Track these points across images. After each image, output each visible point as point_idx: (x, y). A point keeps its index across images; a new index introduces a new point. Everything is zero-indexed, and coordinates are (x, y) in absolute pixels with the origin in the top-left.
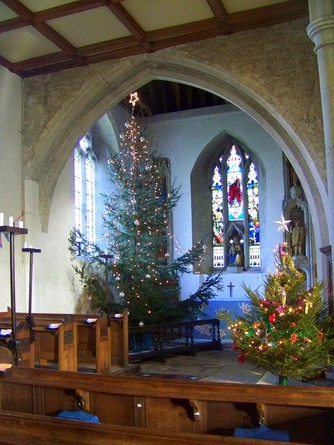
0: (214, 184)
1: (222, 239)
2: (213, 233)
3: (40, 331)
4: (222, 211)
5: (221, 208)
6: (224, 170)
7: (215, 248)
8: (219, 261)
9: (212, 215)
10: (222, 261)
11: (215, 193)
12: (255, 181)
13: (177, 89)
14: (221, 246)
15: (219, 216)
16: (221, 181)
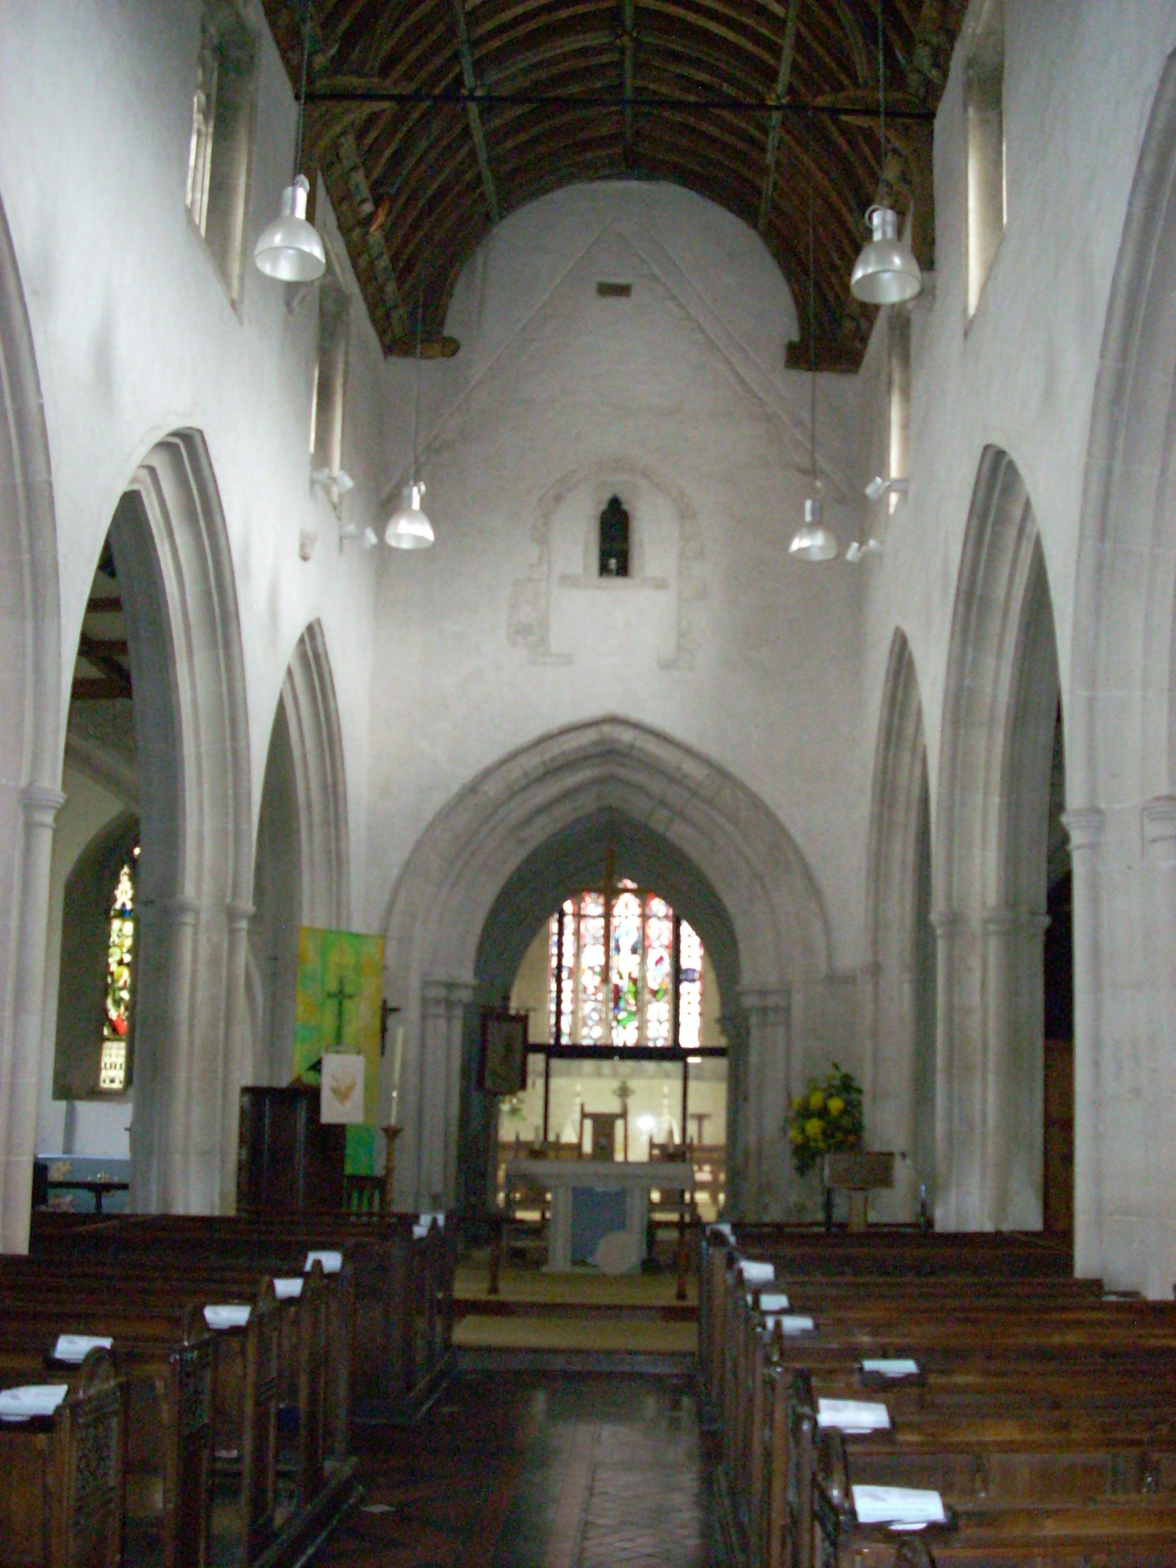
0: (118, 906)
1: (124, 1026)
3: (125, 1432)
4: (128, 965)
5: (127, 958)
6: (789, 1311)
7: (107, 1044)
10: (120, 1075)
11: (116, 924)
12: (129, 906)
13: (78, 703)
14: (119, 1040)
16: (132, 900)
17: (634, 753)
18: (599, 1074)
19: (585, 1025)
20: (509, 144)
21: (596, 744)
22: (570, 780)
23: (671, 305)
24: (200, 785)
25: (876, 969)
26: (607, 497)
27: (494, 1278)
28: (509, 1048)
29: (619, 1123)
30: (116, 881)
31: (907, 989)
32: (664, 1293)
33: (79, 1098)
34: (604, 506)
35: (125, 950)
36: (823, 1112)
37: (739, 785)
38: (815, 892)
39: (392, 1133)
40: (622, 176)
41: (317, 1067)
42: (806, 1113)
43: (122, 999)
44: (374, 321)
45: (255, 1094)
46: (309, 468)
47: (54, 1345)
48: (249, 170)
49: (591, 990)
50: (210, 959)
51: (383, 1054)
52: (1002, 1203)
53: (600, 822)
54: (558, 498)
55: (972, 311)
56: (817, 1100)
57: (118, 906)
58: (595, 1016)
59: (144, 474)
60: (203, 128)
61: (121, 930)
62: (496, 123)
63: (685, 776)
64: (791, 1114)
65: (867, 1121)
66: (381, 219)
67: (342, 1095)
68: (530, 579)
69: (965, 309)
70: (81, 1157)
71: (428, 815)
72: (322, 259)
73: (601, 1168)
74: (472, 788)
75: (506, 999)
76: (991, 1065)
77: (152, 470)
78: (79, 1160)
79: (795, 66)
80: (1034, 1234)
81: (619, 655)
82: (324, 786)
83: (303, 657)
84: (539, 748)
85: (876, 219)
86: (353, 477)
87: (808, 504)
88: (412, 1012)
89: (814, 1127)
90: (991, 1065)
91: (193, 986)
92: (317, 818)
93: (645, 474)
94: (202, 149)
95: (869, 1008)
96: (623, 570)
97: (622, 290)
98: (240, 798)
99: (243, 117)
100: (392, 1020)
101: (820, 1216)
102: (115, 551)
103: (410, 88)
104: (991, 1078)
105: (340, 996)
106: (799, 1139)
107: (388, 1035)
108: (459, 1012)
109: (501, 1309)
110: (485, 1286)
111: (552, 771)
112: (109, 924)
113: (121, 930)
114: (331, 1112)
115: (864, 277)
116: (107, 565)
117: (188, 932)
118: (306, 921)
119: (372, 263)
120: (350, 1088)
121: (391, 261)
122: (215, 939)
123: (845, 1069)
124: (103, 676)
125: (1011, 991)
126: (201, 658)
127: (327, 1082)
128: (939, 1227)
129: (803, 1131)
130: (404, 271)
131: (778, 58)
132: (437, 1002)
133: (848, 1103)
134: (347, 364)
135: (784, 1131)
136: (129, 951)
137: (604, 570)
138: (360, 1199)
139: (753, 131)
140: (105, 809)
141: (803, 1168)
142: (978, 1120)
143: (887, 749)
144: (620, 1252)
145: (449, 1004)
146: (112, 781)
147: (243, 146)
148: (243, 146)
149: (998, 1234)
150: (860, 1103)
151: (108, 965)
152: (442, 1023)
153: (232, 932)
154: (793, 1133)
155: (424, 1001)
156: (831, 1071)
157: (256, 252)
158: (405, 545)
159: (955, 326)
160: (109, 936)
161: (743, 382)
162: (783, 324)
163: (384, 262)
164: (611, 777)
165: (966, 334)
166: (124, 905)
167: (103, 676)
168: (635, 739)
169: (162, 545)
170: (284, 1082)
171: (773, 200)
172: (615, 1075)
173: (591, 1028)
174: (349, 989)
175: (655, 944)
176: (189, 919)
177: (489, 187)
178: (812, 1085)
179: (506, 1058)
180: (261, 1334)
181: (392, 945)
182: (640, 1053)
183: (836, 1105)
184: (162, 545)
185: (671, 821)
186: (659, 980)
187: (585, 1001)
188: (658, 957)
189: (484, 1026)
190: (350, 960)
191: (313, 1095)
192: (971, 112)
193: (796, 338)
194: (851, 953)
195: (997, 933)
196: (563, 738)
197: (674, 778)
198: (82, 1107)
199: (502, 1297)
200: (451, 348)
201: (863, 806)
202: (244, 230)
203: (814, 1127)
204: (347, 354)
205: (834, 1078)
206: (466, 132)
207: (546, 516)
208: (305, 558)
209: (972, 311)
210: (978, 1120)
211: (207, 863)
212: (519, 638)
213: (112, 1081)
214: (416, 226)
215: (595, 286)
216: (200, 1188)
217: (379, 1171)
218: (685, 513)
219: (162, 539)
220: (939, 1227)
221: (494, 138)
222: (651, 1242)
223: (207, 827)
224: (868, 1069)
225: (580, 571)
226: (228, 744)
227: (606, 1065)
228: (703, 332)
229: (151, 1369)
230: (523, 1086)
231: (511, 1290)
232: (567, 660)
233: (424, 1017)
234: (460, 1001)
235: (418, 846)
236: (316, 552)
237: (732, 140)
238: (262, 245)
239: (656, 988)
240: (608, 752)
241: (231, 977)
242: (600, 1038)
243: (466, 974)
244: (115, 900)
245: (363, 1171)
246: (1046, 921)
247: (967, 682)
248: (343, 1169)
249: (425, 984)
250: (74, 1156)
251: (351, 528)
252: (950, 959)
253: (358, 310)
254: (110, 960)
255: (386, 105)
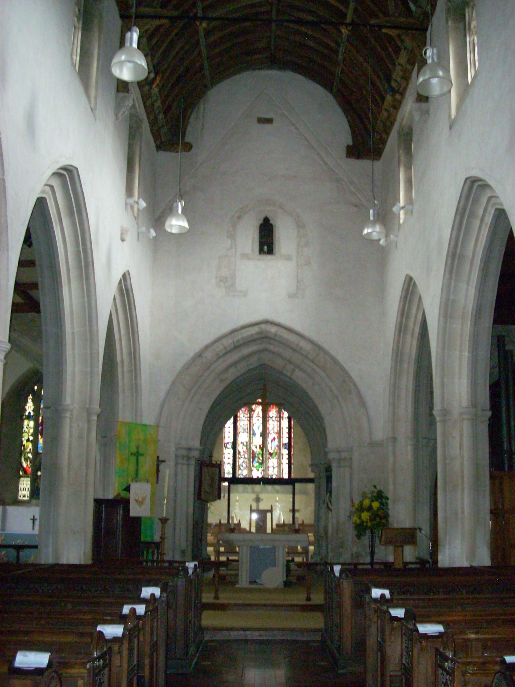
0: (27, 413)
1: (29, 470)
2: (21, 464)
4: (32, 441)
5: (31, 438)
7: (22, 479)
8: (24, 493)
9: (22, 445)
10: (27, 493)
11: (26, 422)
12: (32, 414)
14: (28, 477)
15: (30, 446)
17: (277, 338)
18: (244, 491)
19: (240, 469)
20: (217, 50)
21: (258, 333)
22: (246, 351)
23: (292, 128)
24: (73, 349)
25: (394, 439)
26: (262, 217)
27: (217, 592)
28: (212, 479)
29: (269, 515)
30: (26, 402)
31: (410, 449)
32: (298, 597)
33: (9, 505)
34: (261, 222)
35: (30, 434)
36: (370, 508)
37: (326, 352)
38: (363, 403)
39: (164, 521)
40: (269, 68)
41: (128, 489)
42: (361, 509)
43: (29, 457)
44: (152, 133)
45: (98, 502)
46: (125, 197)
47: (14, 657)
48: (99, 48)
49: (242, 453)
50: (76, 435)
51: (157, 482)
52: (473, 553)
53: (259, 372)
54: (239, 218)
55: (453, 117)
56: (366, 503)
57: (27, 413)
58: (244, 465)
59: (48, 189)
60: (77, 25)
61: (28, 425)
62: (211, 39)
63: (301, 348)
64: (354, 509)
65: (390, 513)
66: (158, 81)
67: (140, 503)
68: (226, 256)
69: (450, 116)
70: (9, 532)
71: (179, 368)
72: (146, 67)
73: (260, 536)
74: (199, 355)
75: (211, 456)
76: (466, 485)
77: (52, 187)
78: (9, 534)
79: (355, 10)
80: (488, 567)
81: (270, 292)
82: (130, 354)
83: (120, 289)
84: (233, 335)
85: (429, 53)
86: (146, 202)
87: (371, 212)
88: (171, 462)
89: (365, 516)
90: (466, 485)
91: (70, 448)
92: (126, 368)
93: (281, 207)
94: (76, 34)
95: (391, 460)
96: (270, 252)
97: (269, 121)
98: (93, 354)
99: (96, 21)
100: (162, 466)
101: (368, 560)
102: (32, 231)
103: (175, 13)
104: (466, 491)
105: (137, 455)
106: (358, 521)
107: (160, 474)
108: (193, 462)
109: (222, 607)
110: (213, 595)
111: (236, 347)
112: (23, 422)
113: (28, 425)
114: (134, 511)
115: (423, 81)
116: (28, 240)
117: (68, 421)
118: (121, 419)
119: (153, 105)
120: (144, 499)
121: (162, 103)
122: (81, 426)
123: (378, 488)
124: (23, 301)
125: (475, 449)
126: (74, 285)
127: (132, 496)
128: (440, 565)
129: (360, 517)
130: (167, 111)
131: (347, 7)
132: (183, 457)
133: (382, 504)
134: (140, 151)
135: (350, 517)
136: (32, 435)
137: (261, 251)
138: (148, 553)
139: (333, 45)
140: (24, 366)
141: (359, 536)
142: (460, 511)
143: (399, 336)
144: (273, 577)
145: (189, 458)
146: (26, 353)
147: (96, 35)
148: (96, 35)
149: (472, 567)
150: (387, 504)
151: (22, 442)
152: (185, 467)
153: (89, 421)
154: (355, 518)
155: (176, 456)
156: (373, 489)
157: (112, 63)
158: (174, 231)
159: (444, 125)
160: (23, 428)
161: (326, 164)
162: (345, 137)
163: (158, 104)
164: (265, 350)
165: (451, 128)
166: (30, 413)
167: (23, 301)
168: (277, 331)
169: (56, 226)
170: (111, 496)
171: (341, 79)
172: (253, 492)
173: (242, 471)
174: (141, 451)
175: (272, 432)
176: (68, 414)
177: (207, 72)
178: (364, 496)
179: (211, 486)
180: (130, 641)
181: (161, 430)
182: (266, 481)
183: (376, 505)
184: (56, 226)
185: (294, 370)
186: (273, 448)
187: (240, 458)
188: (272, 438)
189: (201, 470)
190: (142, 437)
191: (126, 503)
192: (450, 23)
193: (351, 143)
194: (380, 433)
195: (468, 419)
196: (243, 331)
197: (295, 350)
198: (10, 509)
199: (221, 601)
200: (188, 147)
201: (388, 362)
202: (97, 75)
203: (365, 516)
204: (141, 147)
205: (375, 492)
206: (198, 42)
207: (234, 226)
208: (123, 240)
209: (453, 117)
210: (460, 511)
211: (77, 387)
212: (222, 284)
213: (24, 496)
214: (174, 85)
215: (256, 119)
216: (74, 549)
217: (157, 538)
218: (300, 225)
219: (56, 224)
220: (440, 565)
221: (210, 47)
222: (288, 570)
223: (77, 369)
224: (391, 487)
225: (250, 251)
226: (88, 328)
227: (249, 487)
228: (307, 140)
229: (75, 671)
230: (219, 498)
231: (225, 598)
232: (245, 294)
233: (176, 464)
234: (194, 457)
235: (173, 383)
236: (128, 237)
237: (320, 48)
238: (115, 60)
239: (271, 451)
240: (264, 337)
241: (88, 444)
242: (247, 475)
243: (196, 444)
244: (26, 410)
245: (149, 539)
246: (489, 414)
247: (451, 297)
248: (140, 539)
249: (177, 449)
250: (6, 532)
251: (143, 229)
252: (444, 434)
253: (146, 126)
254: (23, 439)
255: (164, 21)
